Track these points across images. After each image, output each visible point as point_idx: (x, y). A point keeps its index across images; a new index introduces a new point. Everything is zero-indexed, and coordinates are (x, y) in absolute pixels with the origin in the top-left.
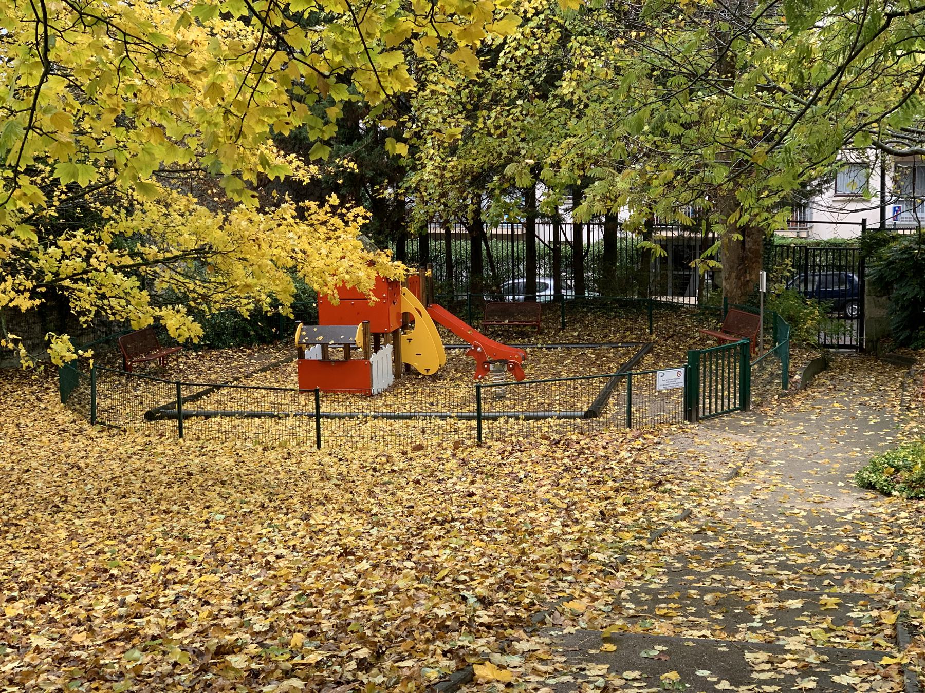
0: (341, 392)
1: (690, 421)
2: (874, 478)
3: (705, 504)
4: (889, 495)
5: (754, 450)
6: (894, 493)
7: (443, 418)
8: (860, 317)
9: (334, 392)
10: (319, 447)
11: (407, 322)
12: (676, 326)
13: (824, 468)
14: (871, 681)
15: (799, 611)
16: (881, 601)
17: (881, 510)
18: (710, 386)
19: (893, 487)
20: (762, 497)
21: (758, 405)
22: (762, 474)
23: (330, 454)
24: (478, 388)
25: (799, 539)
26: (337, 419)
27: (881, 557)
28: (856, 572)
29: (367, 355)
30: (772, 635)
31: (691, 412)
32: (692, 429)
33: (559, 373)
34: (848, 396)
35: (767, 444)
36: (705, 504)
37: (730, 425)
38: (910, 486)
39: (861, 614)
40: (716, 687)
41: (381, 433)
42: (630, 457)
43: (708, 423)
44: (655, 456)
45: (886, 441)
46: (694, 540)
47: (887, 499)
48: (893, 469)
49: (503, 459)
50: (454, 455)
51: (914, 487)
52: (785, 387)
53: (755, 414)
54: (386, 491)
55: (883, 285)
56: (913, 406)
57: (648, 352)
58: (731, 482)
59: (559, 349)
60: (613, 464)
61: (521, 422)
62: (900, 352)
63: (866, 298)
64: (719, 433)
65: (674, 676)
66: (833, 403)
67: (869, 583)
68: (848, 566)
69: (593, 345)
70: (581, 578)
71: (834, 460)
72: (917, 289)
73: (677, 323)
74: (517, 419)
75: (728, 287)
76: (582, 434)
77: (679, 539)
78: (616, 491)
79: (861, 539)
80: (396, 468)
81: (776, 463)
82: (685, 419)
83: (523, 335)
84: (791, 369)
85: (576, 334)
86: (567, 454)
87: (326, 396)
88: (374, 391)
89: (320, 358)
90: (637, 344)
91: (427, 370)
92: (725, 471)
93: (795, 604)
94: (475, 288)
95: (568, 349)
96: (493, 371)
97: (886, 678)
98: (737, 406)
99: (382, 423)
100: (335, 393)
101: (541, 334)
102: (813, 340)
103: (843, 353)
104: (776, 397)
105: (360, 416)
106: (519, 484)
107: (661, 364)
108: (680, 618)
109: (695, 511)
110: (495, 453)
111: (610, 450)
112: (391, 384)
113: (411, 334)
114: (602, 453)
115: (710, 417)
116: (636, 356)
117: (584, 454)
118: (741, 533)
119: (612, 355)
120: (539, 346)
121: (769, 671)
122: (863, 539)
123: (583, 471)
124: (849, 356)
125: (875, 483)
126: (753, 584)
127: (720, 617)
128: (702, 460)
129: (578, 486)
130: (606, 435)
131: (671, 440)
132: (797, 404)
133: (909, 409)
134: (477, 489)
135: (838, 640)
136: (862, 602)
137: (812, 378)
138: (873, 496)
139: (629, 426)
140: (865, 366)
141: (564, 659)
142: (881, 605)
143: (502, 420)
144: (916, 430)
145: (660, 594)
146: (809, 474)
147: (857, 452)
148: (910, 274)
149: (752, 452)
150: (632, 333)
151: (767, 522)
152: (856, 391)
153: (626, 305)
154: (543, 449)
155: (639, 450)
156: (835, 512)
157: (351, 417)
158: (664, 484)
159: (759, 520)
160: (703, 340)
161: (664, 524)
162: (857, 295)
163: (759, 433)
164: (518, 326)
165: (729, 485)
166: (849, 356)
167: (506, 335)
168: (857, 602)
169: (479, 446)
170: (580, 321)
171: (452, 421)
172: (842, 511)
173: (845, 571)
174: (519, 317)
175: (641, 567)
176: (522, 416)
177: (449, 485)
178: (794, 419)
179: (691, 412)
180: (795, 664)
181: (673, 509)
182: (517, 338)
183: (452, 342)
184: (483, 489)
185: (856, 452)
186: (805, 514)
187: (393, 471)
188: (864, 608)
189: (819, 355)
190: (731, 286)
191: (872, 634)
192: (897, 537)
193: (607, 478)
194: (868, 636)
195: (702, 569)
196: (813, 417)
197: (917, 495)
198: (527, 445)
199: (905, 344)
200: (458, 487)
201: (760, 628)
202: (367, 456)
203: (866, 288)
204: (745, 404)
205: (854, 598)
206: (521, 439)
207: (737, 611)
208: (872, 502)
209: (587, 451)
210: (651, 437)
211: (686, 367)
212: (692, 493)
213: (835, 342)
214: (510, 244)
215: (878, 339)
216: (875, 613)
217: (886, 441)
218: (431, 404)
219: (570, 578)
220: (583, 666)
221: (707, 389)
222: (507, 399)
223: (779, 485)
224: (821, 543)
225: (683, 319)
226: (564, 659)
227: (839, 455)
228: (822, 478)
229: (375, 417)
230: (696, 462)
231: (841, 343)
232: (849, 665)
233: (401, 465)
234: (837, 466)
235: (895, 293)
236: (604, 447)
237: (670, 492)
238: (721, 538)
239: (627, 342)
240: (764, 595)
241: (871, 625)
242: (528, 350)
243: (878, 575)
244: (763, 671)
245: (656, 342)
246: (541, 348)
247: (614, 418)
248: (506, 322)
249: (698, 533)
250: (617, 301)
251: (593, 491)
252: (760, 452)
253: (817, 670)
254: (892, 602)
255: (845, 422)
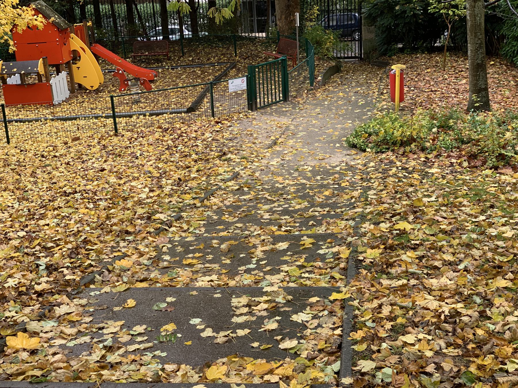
0: (33, 104)
1: (252, 110)
2: (356, 141)
3: (249, 167)
4: (364, 151)
5: (289, 126)
6: (368, 150)
7: (96, 118)
8: (360, 40)
9: (28, 104)
10: (8, 142)
11: (76, 57)
12: (252, 50)
13: (330, 136)
14: (320, 317)
15: (285, 251)
16: (342, 238)
17: (359, 161)
18: (267, 87)
19: (367, 146)
20: (287, 159)
21: (295, 97)
22: (291, 142)
23: (16, 147)
24: (112, 97)
25: (303, 188)
26: (27, 123)
27: (352, 198)
28: (333, 213)
29: (48, 80)
30: (262, 274)
31: (252, 105)
32: (253, 115)
33: (177, 84)
34: (348, 88)
35: (297, 122)
36: (249, 167)
37: (276, 111)
38: (377, 145)
39: (327, 251)
40: (202, 335)
41: (55, 130)
42: (211, 137)
43: (263, 111)
44: (227, 135)
45: (367, 115)
46: (234, 195)
47: (363, 154)
48: (367, 135)
49: (130, 143)
50: (99, 143)
51: (380, 145)
52: (312, 85)
53: (292, 103)
54: (44, 172)
55: (372, 18)
56: (385, 92)
57: (233, 68)
58: (270, 149)
59: (179, 69)
60: (199, 143)
61: (147, 117)
62: (381, 59)
63: (363, 28)
64: (269, 117)
65: (171, 327)
66: (339, 93)
67: (338, 222)
68: (327, 209)
69: (201, 65)
70: (139, 238)
71: (335, 129)
72: (390, 20)
73: (253, 48)
74: (145, 115)
75: (280, 25)
76: (183, 123)
77: (224, 195)
78: (196, 161)
79: (342, 185)
80: (57, 154)
81: (301, 134)
82: (249, 109)
83: (158, 61)
84: (316, 73)
85: (191, 59)
86: (171, 137)
87: (23, 108)
88: (55, 102)
89: (19, 82)
90: (226, 63)
91: (92, 87)
92: (268, 142)
93: (283, 246)
94: (133, 33)
95: (185, 69)
96: (132, 86)
97: (332, 313)
98: (281, 98)
99: (56, 124)
100: (29, 105)
101: (169, 60)
102: (331, 54)
103: (351, 62)
104: (306, 91)
105: (42, 120)
106: (136, 161)
107: (240, 75)
108: (200, 266)
109: (242, 173)
110: (126, 140)
111: (199, 133)
112: (68, 97)
113: (79, 64)
114: (194, 135)
115: (264, 107)
116: (225, 71)
117: (182, 136)
118: (266, 187)
119: (211, 71)
120: (167, 67)
121: (245, 314)
122: (343, 185)
123: (179, 148)
124: (354, 63)
125: (356, 144)
126: (261, 229)
127: (228, 261)
128: (255, 136)
129: (172, 159)
130: (198, 123)
131: (238, 124)
132: (318, 95)
133: (382, 94)
134: (108, 165)
135: (307, 275)
136: (329, 240)
137: (329, 78)
138: (355, 152)
139: (213, 116)
140: (362, 69)
141: (91, 319)
142: (341, 241)
143: (135, 117)
144: (385, 107)
145: (192, 246)
146: (320, 140)
147: (350, 123)
148: (386, 11)
149: (287, 128)
150: (224, 57)
151: (287, 176)
152: (354, 84)
153: (221, 39)
154: (157, 135)
155: (217, 131)
156: (330, 166)
157: (37, 120)
158: (227, 155)
159: (281, 175)
160: (266, 59)
161: (217, 184)
162: (358, 27)
163: (293, 115)
164: (155, 55)
165: (268, 152)
166: (354, 63)
167: (148, 62)
168: (326, 240)
169: (116, 135)
170: (194, 50)
171: (102, 120)
172: (334, 165)
173: (325, 213)
174: (158, 50)
175: (188, 223)
176: (148, 114)
177: (90, 164)
178: (315, 105)
179: (252, 105)
180: (265, 306)
181: (227, 172)
182: (155, 63)
183: (113, 68)
184: (111, 165)
185: (349, 124)
186: (311, 169)
187: (55, 156)
188: (330, 245)
189: (334, 64)
190: (282, 24)
191: (331, 268)
192: (364, 182)
193: (192, 152)
194: (329, 270)
195: (231, 219)
196: (326, 103)
197: (381, 150)
198: (148, 133)
199: (384, 54)
200: (95, 165)
201: (254, 269)
202: (41, 147)
203: (363, 21)
204: (286, 98)
205: (323, 237)
206: (143, 129)
207: (242, 256)
208: (354, 156)
209: (184, 135)
210: (226, 122)
211: (247, 76)
212: (242, 160)
213: (342, 55)
214: (151, 4)
215: (370, 52)
216: (335, 250)
217: (367, 115)
218: (92, 109)
219: (131, 238)
220: (101, 325)
221: (266, 89)
222: (142, 103)
223: (299, 149)
224: (316, 190)
225: (257, 46)
226: (91, 319)
227: (339, 126)
228: (329, 143)
229: (52, 120)
230: (251, 138)
231: (346, 56)
232: (307, 302)
233: (62, 152)
234: (337, 133)
235: (378, 24)
236: (196, 131)
237: (229, 160)
238: (252, 192)
239: (222, 62)
240: (264, 240)
241: (332, 260)
242: (160, 70)
243: (346, 215)
244: (241, 315)
245: (238, 61)
246: (168, 69)
247: (206, 111)
248: (147, 53)
249: (238, 189)
250: (217, 37)
251: (180, 163)
252: (292, 127)
253: (282, 310)
254: (349, 239)
255: (344, 105)
